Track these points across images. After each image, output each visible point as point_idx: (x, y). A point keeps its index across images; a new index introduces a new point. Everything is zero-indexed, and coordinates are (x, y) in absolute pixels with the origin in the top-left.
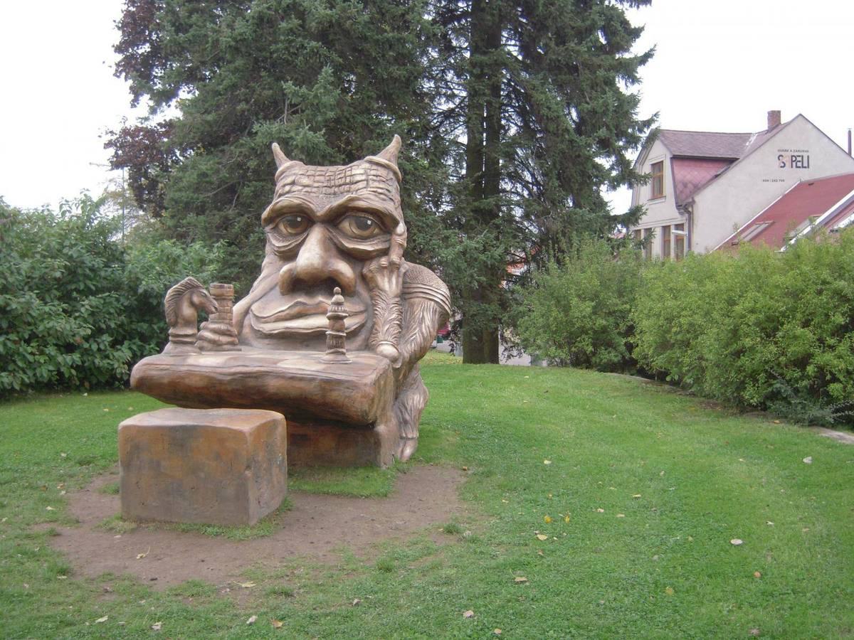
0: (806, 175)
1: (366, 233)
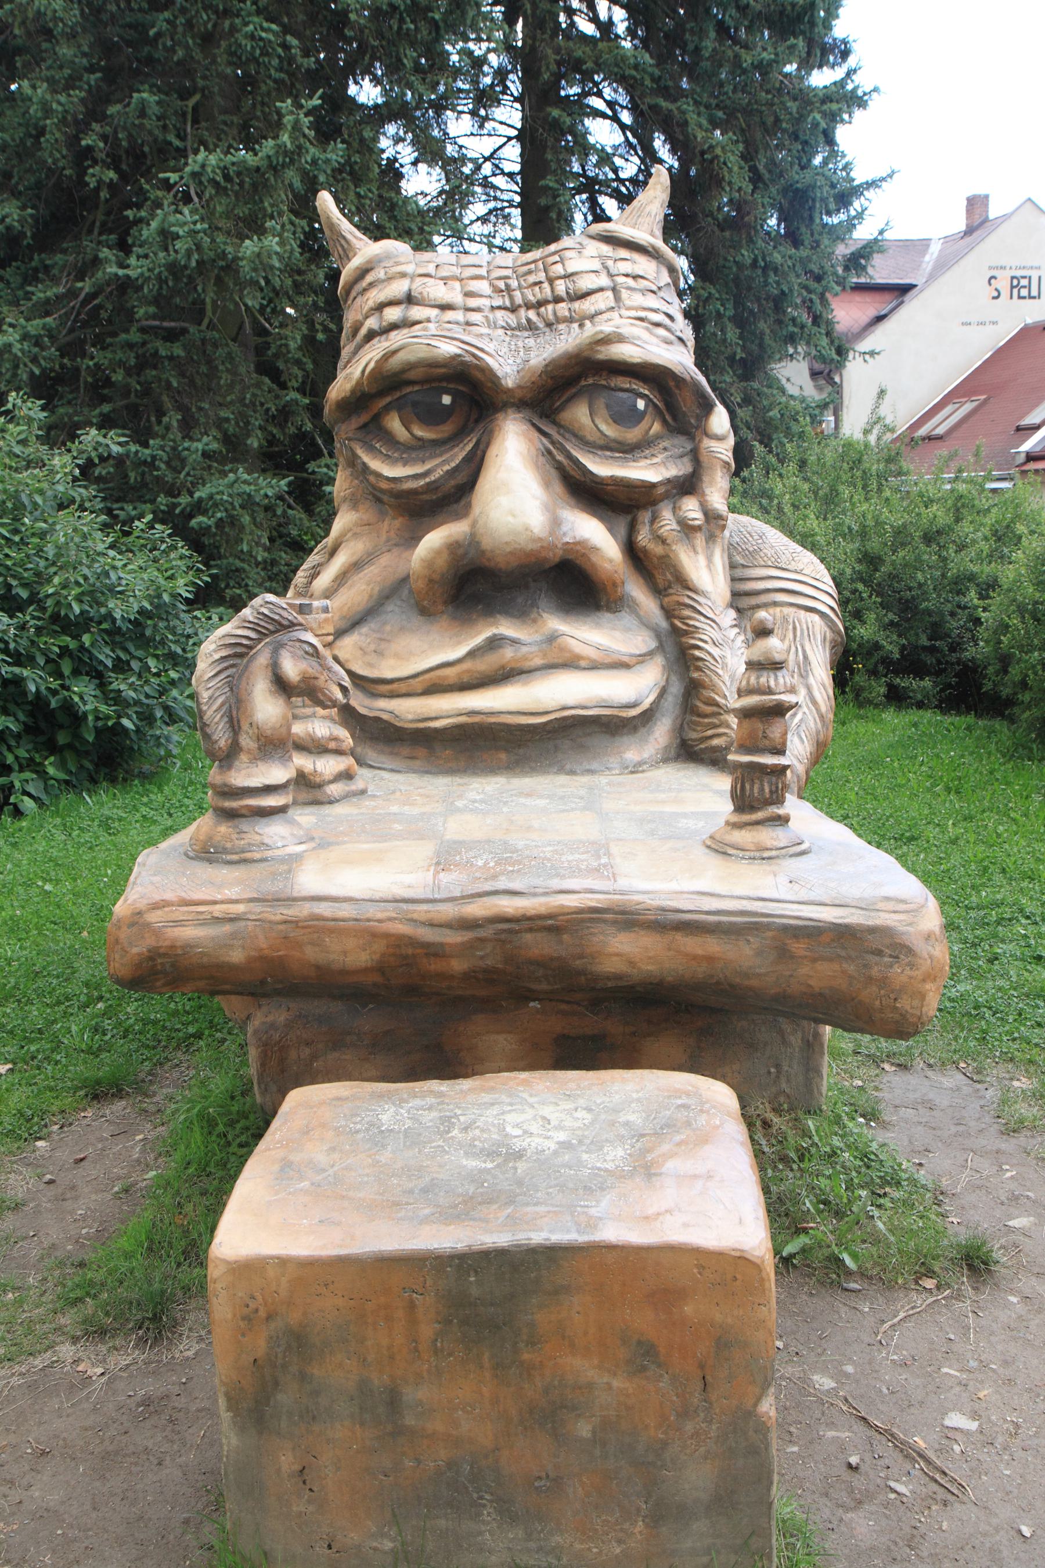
0: (1032, 313)
1: (633, 435)
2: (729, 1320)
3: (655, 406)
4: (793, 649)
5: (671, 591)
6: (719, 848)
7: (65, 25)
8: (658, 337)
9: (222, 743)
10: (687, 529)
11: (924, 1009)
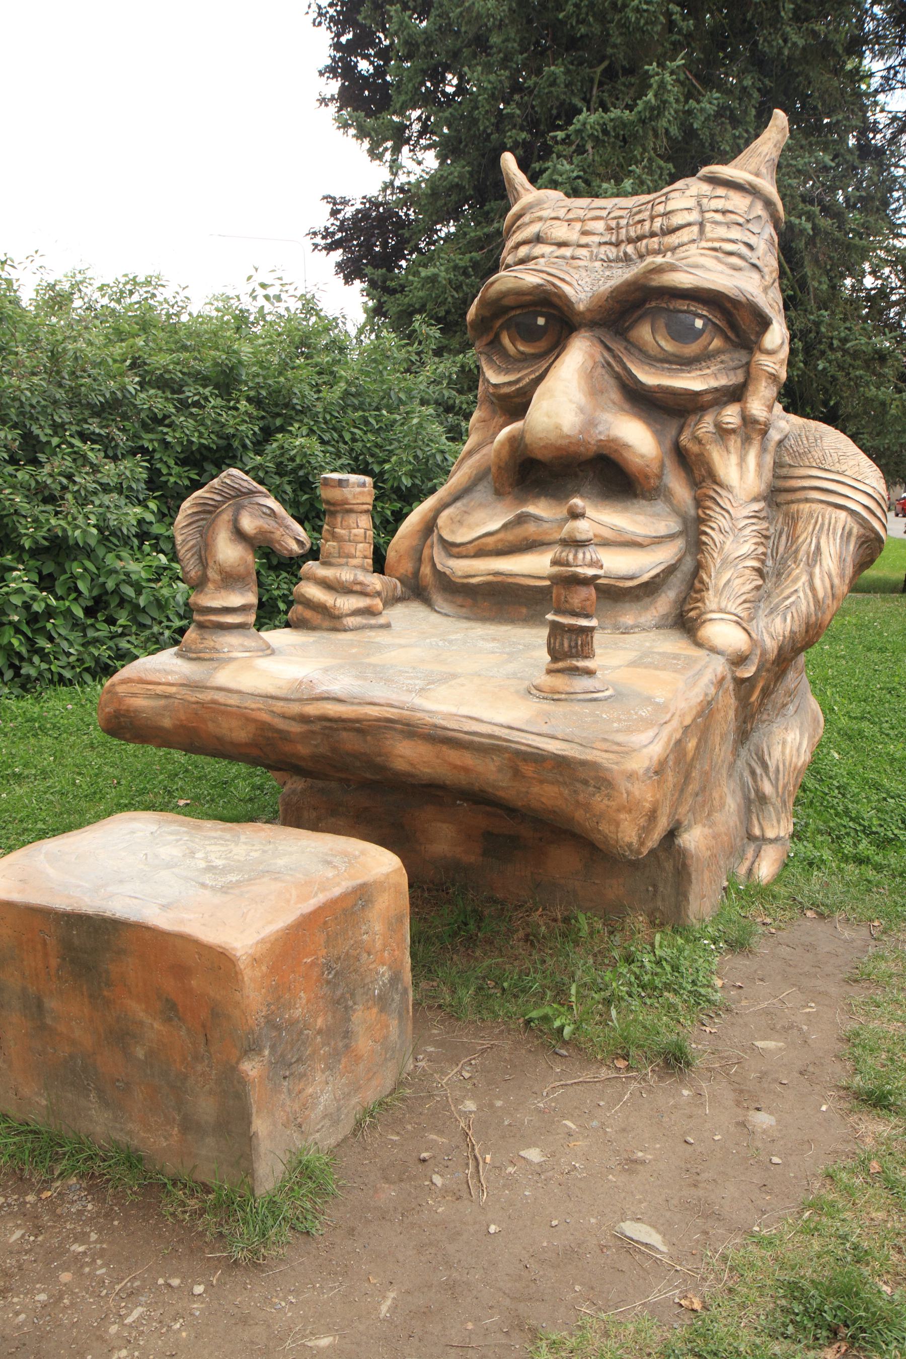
1: (691, 349)
2: (218, 997)
3: (714, 324)
4: (809, 540)
5: (704, 484)
6: (536, 692)
7: (495, 19)
8: (726, 264)
9: (193, 574)
10: (723, 432)
11: (620, 835)
